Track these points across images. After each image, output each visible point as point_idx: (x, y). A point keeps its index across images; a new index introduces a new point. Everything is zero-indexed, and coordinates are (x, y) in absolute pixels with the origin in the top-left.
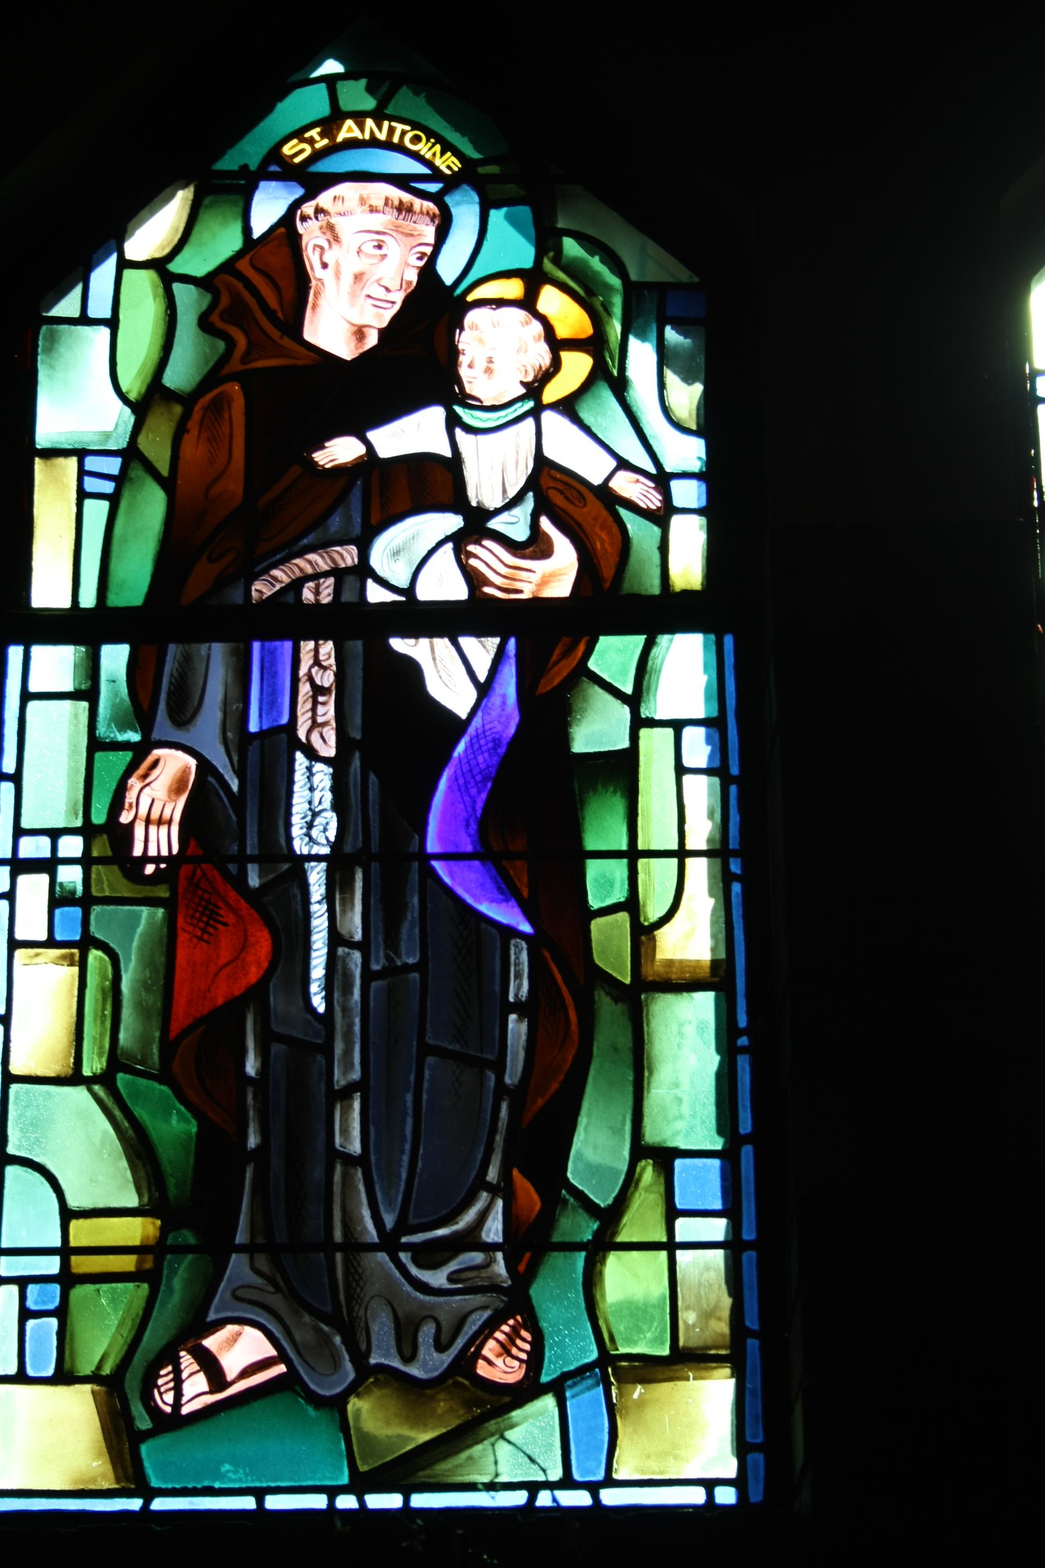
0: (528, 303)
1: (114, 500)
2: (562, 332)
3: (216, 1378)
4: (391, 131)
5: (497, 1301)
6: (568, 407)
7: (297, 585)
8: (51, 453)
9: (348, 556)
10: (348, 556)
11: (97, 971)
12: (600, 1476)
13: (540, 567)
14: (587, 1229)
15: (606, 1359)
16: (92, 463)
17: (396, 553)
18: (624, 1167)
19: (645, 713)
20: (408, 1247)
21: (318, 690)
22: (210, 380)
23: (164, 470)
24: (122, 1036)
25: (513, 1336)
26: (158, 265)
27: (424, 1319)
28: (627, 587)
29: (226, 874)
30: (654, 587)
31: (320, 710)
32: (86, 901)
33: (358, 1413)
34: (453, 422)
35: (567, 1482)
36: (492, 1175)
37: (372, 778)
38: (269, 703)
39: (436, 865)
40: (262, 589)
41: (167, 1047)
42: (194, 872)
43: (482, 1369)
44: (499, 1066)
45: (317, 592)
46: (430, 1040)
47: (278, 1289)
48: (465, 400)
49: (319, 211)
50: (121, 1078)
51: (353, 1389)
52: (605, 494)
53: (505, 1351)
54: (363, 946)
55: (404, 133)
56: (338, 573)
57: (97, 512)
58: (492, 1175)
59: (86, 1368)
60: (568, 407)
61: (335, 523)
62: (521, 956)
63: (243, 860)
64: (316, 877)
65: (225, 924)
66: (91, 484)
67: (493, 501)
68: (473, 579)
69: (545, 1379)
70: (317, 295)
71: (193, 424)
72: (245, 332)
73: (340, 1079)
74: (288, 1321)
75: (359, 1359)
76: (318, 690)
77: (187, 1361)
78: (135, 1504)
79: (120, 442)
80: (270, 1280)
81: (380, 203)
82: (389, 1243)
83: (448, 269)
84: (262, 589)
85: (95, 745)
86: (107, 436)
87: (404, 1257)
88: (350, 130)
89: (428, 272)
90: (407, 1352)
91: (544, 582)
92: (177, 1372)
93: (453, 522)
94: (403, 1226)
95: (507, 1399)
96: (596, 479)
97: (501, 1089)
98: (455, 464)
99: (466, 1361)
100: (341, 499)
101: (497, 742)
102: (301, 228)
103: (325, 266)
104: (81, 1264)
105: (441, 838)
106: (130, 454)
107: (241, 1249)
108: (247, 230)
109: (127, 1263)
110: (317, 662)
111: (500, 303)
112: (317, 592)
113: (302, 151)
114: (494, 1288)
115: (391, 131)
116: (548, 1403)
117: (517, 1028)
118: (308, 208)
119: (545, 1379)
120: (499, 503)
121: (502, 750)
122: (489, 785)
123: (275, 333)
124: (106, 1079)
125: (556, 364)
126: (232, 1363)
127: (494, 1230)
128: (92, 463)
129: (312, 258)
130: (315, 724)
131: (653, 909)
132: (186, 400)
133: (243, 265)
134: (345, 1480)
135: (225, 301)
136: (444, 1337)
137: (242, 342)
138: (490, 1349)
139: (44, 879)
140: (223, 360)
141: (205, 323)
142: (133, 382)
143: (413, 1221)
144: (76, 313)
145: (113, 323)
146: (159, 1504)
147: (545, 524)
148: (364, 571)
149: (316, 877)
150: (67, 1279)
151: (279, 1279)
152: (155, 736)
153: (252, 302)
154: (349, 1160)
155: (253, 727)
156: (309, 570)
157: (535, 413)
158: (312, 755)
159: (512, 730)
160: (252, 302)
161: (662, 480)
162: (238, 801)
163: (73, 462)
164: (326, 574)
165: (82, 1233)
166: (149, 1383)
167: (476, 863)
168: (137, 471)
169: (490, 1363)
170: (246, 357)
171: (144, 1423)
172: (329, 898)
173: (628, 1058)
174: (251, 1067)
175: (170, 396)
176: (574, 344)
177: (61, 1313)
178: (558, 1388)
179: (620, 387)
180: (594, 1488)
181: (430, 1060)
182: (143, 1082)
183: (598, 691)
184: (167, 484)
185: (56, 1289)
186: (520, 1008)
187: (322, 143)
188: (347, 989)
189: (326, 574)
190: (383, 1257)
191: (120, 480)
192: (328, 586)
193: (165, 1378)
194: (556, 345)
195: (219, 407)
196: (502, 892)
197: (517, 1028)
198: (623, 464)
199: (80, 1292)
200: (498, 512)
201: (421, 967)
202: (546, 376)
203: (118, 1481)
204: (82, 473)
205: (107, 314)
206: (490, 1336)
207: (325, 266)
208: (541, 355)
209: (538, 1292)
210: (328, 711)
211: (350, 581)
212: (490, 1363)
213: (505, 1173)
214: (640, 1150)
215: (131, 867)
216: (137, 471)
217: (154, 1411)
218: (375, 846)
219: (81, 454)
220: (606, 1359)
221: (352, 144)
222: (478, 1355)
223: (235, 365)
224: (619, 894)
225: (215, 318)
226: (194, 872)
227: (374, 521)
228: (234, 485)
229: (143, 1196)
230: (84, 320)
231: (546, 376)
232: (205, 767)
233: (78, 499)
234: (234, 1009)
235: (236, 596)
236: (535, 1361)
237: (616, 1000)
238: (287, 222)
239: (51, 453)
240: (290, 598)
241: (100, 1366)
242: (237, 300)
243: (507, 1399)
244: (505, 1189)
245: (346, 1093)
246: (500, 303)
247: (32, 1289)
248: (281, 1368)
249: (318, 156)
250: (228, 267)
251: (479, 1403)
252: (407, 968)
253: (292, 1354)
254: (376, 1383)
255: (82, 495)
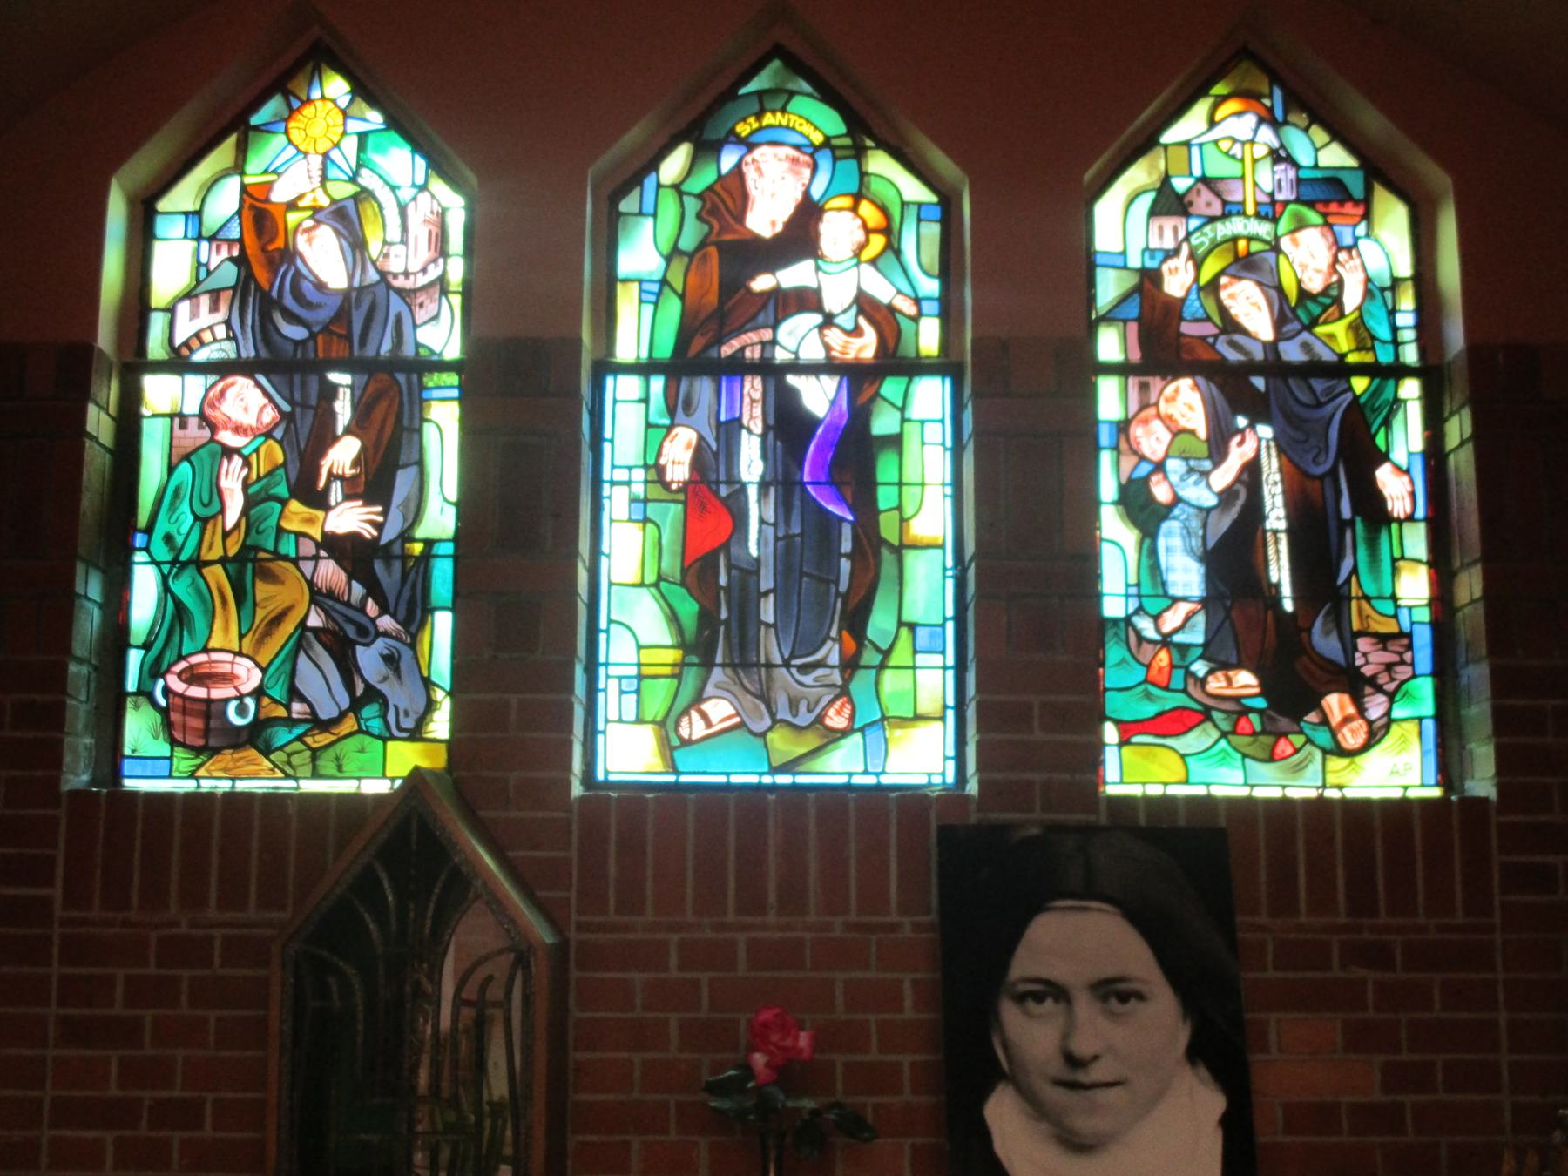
0: (854, 209)
1: (656, 304)
2: (871, 224)
3: (709, 724)
4: (789, 120)
5: (837, 691)
6: (873, 262)
7: (743, 349)
8: (625, 281)
9: (767, 335)
10: (767, 335)
11: (1185, 554)
12: (880, 770)
13: (856, 342)
14: (876, 659)
15: (884, 718)
16: (646, 286)
17: (790, 333)
18: (894, 630)
19: (907, 415)
20: (794, 666)
21: (753, 401)
22: (702, 245)
23: (680, 290)
24: (664, 565)
25: (842, 706)
26: (677, 187)
27: (801, 699)
28: (901, 352)
29: (710, 489)
30: (912, 354)
31: (754, 410)
32: (646, 501)
33: (772, 740)
34: (818, 268)
35: (866, 772)
36: (834, 633)
37: (779, 443)
38: (730, 407)
39: (809, 487)
40: (727, 350)
41: (684, 571)
42: (695, 488)
43: (828, 722)
44: (837, 583)
45: (752, 352)
46: (805, 569)
47: (735, 683)
48: (822, 257)
49: (754, 161)
50: (663, 585)
51: (770, 729)
52: (891, 309)
53: (839, 713)
54: (775, 525)
55: (795, 122)
56: (763, 344)
57: (648, 309)
58: (834, 633)
59: (649, 717)
60: (873, 262)
61: (761, 318)
62: (847, 531)
63: (718, 483)
64: (752, 492)
65: (710, 513)
66: (645, 296)
67: (836, 311)
68: (828, 348)
69: (857, 726)
70: (753, 203)
71: (693, 267)
72: (718, 220)
73: (763, 588)
74: (740, 697)
75: (773, 715)
76: (753, 401)
77: (694, 714)
78: (671, 778)
79: (658, 276)
80: (731, 679)
81: (783, 157)
82: (787, 664)
83: (816, 193)
84: (727, 350)
85: (649, 425)
86: (652, 273)
87: (794, 671)
88: (769, 119)
89: (807, 194)
90: (794, 712)
91: (861, 349)
92: (690, 720)
93: (818, 319)
94: (793, 656)
95: (839, 735)
96: (885, 300)
97: (838, 594)
98: (817, 293)
99: (820, 719)
100: (764, 306)
101: (837, 428)
102: (745, 169)
103: (756, 188)
104: (646, 671)
105: (812, 473)
106: (664, 282)
107: (719, 665)
108: (719, 170)
109: (667, 670)
110: (752, 387)
111: (840, 209)
112: (752, 352)
113: (745, 130)
114: (834, 686)
115: (789, 120)
116: (857, 737)
117: (845, 565)
118: (749, 158)
119: (857, 726)
120: (839, 311)
121: (840, 432)
122: (833, 449)
123: (732, 221)
124: (656, 585)
125: (867, 241)
126: (714, 719)
127: (834, 659)
128: (646, 286)
129: (750, 184)
130: (751, 417)
131: (908, 512)
132: (691, 255)
133: (718, 188)
134: (766, 768)
135: (708, 205)
136: (811, 707)
137: (716, 226)
138: (831, 712)
139: (625, 488)
140: (706, 237)
141: (699, 217)
142: (666, 248)
143: (796, 654)
144: (636, 210)
145: (655, 215)
146: (684, 779)
147: (862, 321)
148: (774, 342)
149: (752, 492)
150: (640, 677)
151: (736, 679)
152: (676, 422)
153: (721, 206)
154: (768, 625)
155: (723, 418)
156: (749, 342)
157: (858, 264)
158: (750, 431)
159: (844, 422)
160: (721, 206)
161: (917, 301)
162: (716, 455)
163: (635, 286)
164: (756, 344)
165: (647, 656)
166: (677, 724)
167: (827, 486)
168: (667, 290)
169: (831, 719)
170: (719, 233)
171: (676, 742)
172: (759, 501)
173: (897, 581)
174: (723, 580)
175: (682, 253)
176: (877, 231)
177: (638, 692)
178: (862, 730)
179: (898, 253)
180: (878, 774)
181: (805, 579)
182: (674, 587)
183: (886, 404)
184: (682, 297)
185: (635, 681)
186: (846, 555)
187: (755, 125)
188: (766, 544)
189: (756, 344)
190: (784, 670)
191: (659, 294)
192: (758, 348)
193: (685, 720)
194: (868, 231)
195: (705, 258)
196: (838, 499)
197: (845, 565)
198: (899, 292)
199: (646, 683)
200: (838, 315)
201: (802, 535)
202: (862, 247)
203: (664, 768)
204: (641, 291)
205: (652, 211)
206: (831, 707)
207: (756, 188)
208: (860, 236)
209: (854, 687)
210: (758, 411)
211: (768, 347)
212: (831, 719)
213: (840, 632)
214: (901, 624)
215: (666, 486)
216: (667, 290)
217: (680, 738)
218: (780, 478)
219: (641, 282)
220: (884, 718)
221: (769, 127)
222: (826, 715)
223: (713, 238)
224: (895, 504)
225: (704, 214)
226: (695, 488)
227: (780, 317)
228: (713, 298)
229: (433, 1034)
230: (641, 213)
231: (862, 247)
232: (701, 438)
233: (814, 720)
234: (714, 554)
235: (713, 353)
236: (852, 718)
237: (892, 553)
238: (738, 171)
239: (625, 281)
240: (740, 355)
241: (655, 717)
242: (714, 205)
243: (839, 735)
244: (839, 639)
245: (766, 594)
246: (840, 209)
247: (624, 681)
248: (737, 720)
249: (753, 132)
250: (710, 188)
251: (826, 737)
252: (795, 536)
253: (742, 713)
254: (781, 726)
255: (641, 301)
